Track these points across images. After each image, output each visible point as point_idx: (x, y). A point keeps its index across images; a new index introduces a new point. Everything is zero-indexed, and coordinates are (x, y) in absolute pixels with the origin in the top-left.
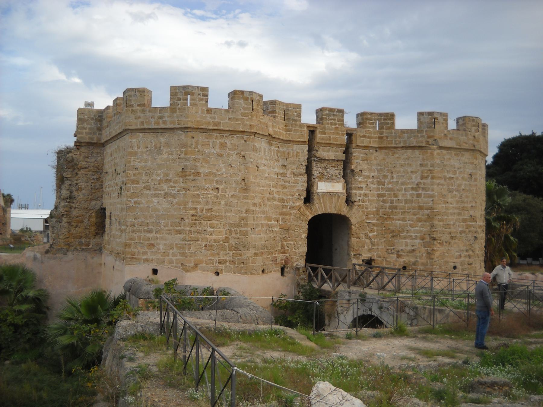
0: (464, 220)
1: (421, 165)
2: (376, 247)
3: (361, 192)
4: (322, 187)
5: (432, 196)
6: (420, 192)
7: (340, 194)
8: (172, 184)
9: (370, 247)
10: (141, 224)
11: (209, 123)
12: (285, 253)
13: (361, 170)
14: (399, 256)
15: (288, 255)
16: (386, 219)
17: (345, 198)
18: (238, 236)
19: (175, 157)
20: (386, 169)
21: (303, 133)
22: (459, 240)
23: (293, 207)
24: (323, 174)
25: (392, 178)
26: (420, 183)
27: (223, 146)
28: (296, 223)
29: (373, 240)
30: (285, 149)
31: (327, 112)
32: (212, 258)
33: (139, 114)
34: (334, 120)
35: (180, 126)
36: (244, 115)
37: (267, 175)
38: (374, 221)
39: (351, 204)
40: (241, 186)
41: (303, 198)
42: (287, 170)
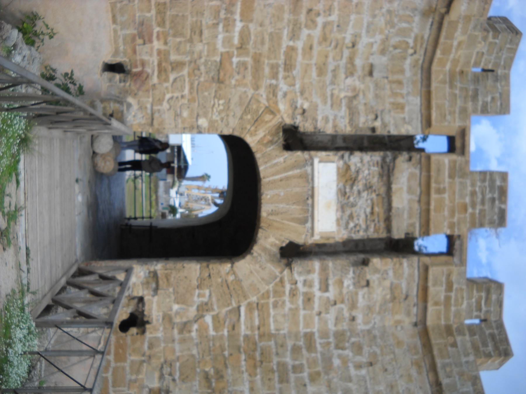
4: (326, 171)
7: (309, 225)
9: (177, 320)
12: (160, 72)
13: (368, 284)
15: (155, 80)
16: (250, 357)
20: (378, 351)
21: (448, 117)
23: (275, 95)
24: (354, 181)
25: (359, 367)
28: (235, 100)
30: (408, 74)
34: (483, 203)
38: (243, 329)
41: (299, 121)
42: (362, 79)
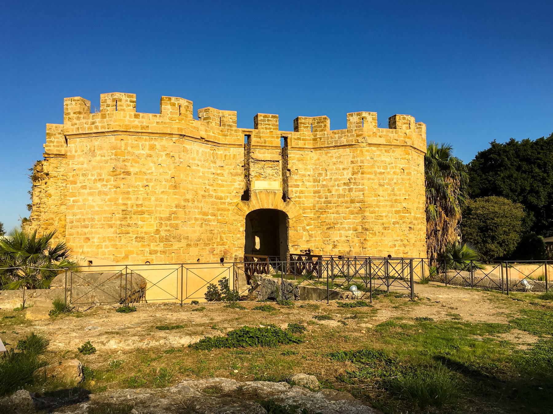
0: (397, 212)
1: (352, 162)
2: (314, 239)
3: (297, 189)
4: (257, 185)
5: (362, 190)
6: (352, 187)
7: (276, 191)
8: (105, 183)
10: (79, 221)
11: (137, 127)
14: (335, 246)
16: (322, 213)
17: (282, 195)
18: (168, 228)
19: (107, 158)
20: (321, 167)
22: (393, 231)
25: (326, 175)
26: (352, 178)
27: (152, 148)
29: (310, 232)
31: (262, 118)
32: (143, 249)
33: (75, 121)
34: (269, 125)
35: (109, 130)
36: (171, 119)
37: (201, 174)
38: (312, 215)
39: (288, 200)
40: (171, 184)
